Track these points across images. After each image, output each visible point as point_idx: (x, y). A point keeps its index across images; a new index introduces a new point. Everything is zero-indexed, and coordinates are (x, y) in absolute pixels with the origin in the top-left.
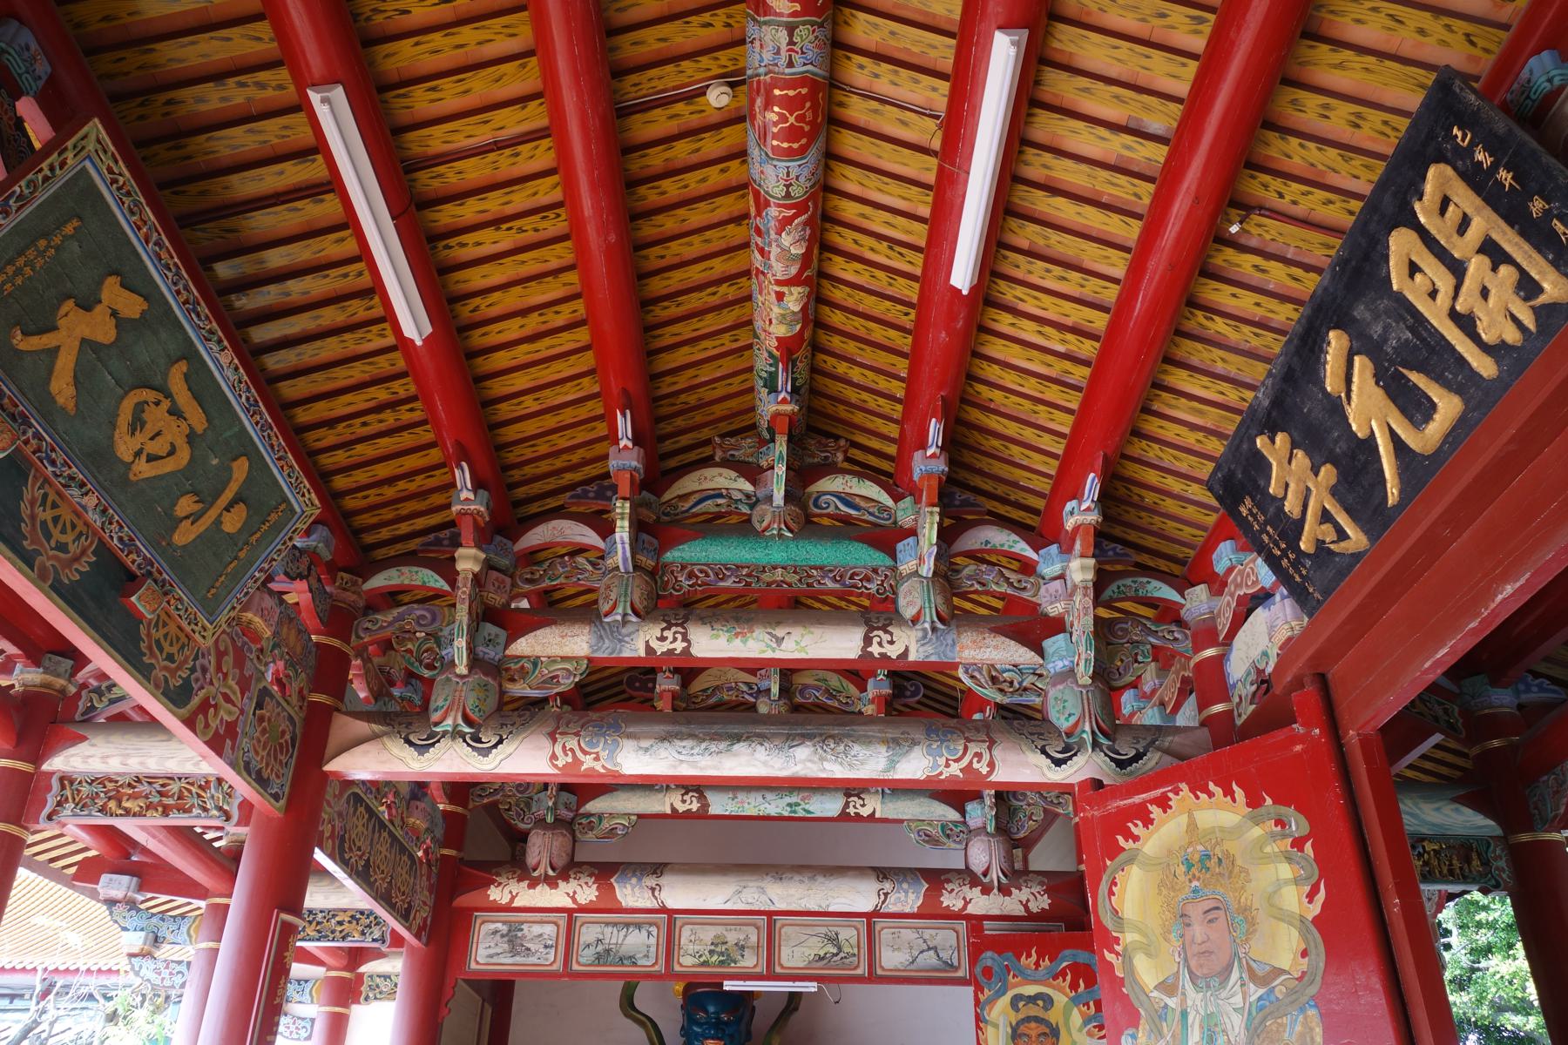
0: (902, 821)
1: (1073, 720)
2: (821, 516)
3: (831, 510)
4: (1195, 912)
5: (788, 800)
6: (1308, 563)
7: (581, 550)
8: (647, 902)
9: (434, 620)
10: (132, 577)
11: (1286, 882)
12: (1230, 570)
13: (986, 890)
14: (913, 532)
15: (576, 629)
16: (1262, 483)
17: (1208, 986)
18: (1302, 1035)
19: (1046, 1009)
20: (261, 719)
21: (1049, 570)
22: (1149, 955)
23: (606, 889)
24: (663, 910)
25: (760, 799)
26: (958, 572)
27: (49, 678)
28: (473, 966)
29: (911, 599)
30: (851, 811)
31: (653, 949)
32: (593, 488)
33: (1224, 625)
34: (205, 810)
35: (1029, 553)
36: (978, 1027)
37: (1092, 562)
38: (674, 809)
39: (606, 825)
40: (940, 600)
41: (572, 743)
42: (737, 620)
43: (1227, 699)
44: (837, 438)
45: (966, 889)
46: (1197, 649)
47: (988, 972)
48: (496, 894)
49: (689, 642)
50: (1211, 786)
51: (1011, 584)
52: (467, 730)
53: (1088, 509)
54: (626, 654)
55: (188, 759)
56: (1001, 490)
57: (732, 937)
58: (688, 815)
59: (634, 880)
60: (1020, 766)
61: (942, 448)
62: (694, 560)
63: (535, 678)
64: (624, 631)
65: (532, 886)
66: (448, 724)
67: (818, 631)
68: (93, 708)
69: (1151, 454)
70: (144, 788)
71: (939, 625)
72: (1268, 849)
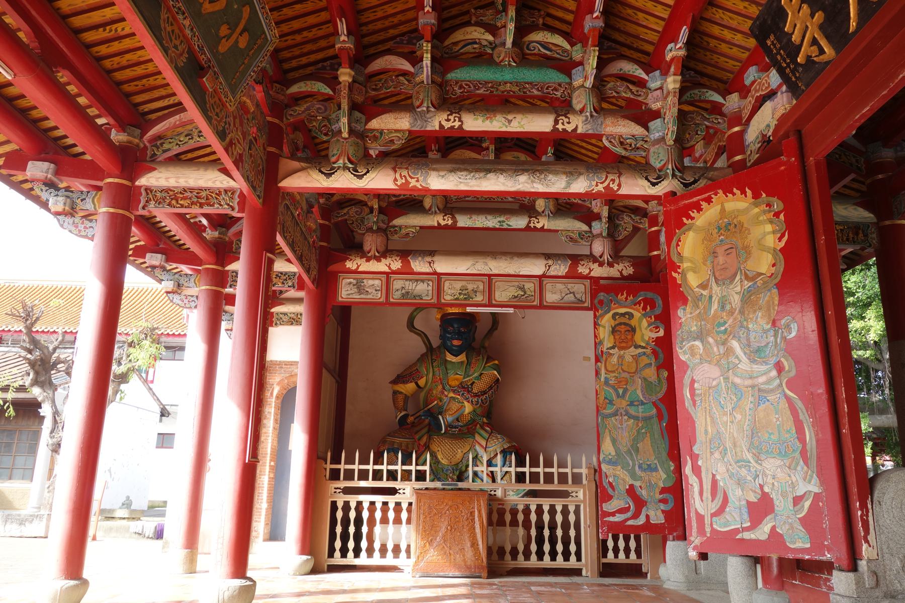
0: (557, 231)
1: (662, 163)
2: (531, 55)
3: (536, 51)
4: (720, 251)
5: (499, 219)
6: (801, 69)
7: (405, 73)
8: (427, 269)
9: (326, 110)
10: (202, 68)
11: (769, 233)
12: (753, 82)
13: (601, 265)
14: (581, 63)
15: (402, 115)
16: (781, 25)
17: (724, 284)
18: (768, 301)
19: (630, 319)
20: (251, 155)
21: (653, 85)
22: (695, 272)
23: (406, 263)
24: (435, 273)
25: (484, 219)
26: (604, 86)
27: (131, 138)
28: (340, 299)
29: (580, 100)
30: (532, 225)
31: (430, 292)
32: (405, 38)
33: (746, 114)
34: (221, 205)
35: (644, 76)
36: (595, 328)
37: (679, 78)
38: (439, 224)
39: (403, 231)
40: (595, 101)
41: (405, 173)
42: (488, 111)
43: (743, 153)
44: (539, 10)
45: (591, 264)
46: (730, 127)
47: (601, 302)
48: (349, 265)
49: (462, 122)
50: (735, 190)
51: (632, 93)
52: (350, 166)
53: (680, 48)
54: (429, 128)
55: (210, 180)
56: (629, 41)
57: (470, 287)
58: (446, 227)
59: (420, 258)
60: (634, 187)
61: (602, 13)
62: (463, 79)
63: (381, 141)
64: (428, 116)
65: (368, 260)
66: (340, 163)
67: (530, 117)
68: (155, 155)
69: (717, 16)
70: (188, 194)
71: (594, 114)
72: (761, 218)
